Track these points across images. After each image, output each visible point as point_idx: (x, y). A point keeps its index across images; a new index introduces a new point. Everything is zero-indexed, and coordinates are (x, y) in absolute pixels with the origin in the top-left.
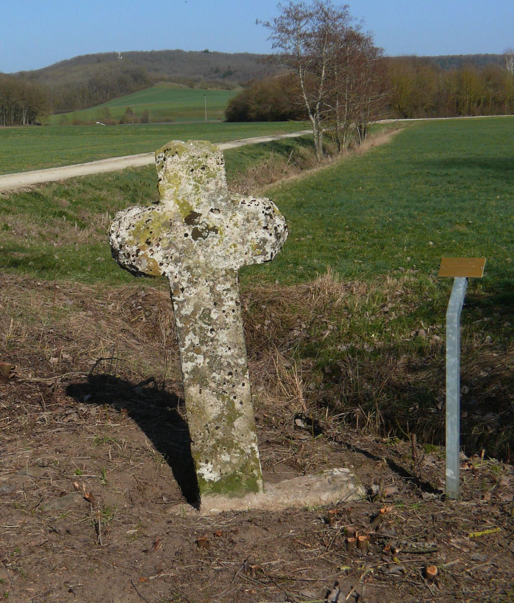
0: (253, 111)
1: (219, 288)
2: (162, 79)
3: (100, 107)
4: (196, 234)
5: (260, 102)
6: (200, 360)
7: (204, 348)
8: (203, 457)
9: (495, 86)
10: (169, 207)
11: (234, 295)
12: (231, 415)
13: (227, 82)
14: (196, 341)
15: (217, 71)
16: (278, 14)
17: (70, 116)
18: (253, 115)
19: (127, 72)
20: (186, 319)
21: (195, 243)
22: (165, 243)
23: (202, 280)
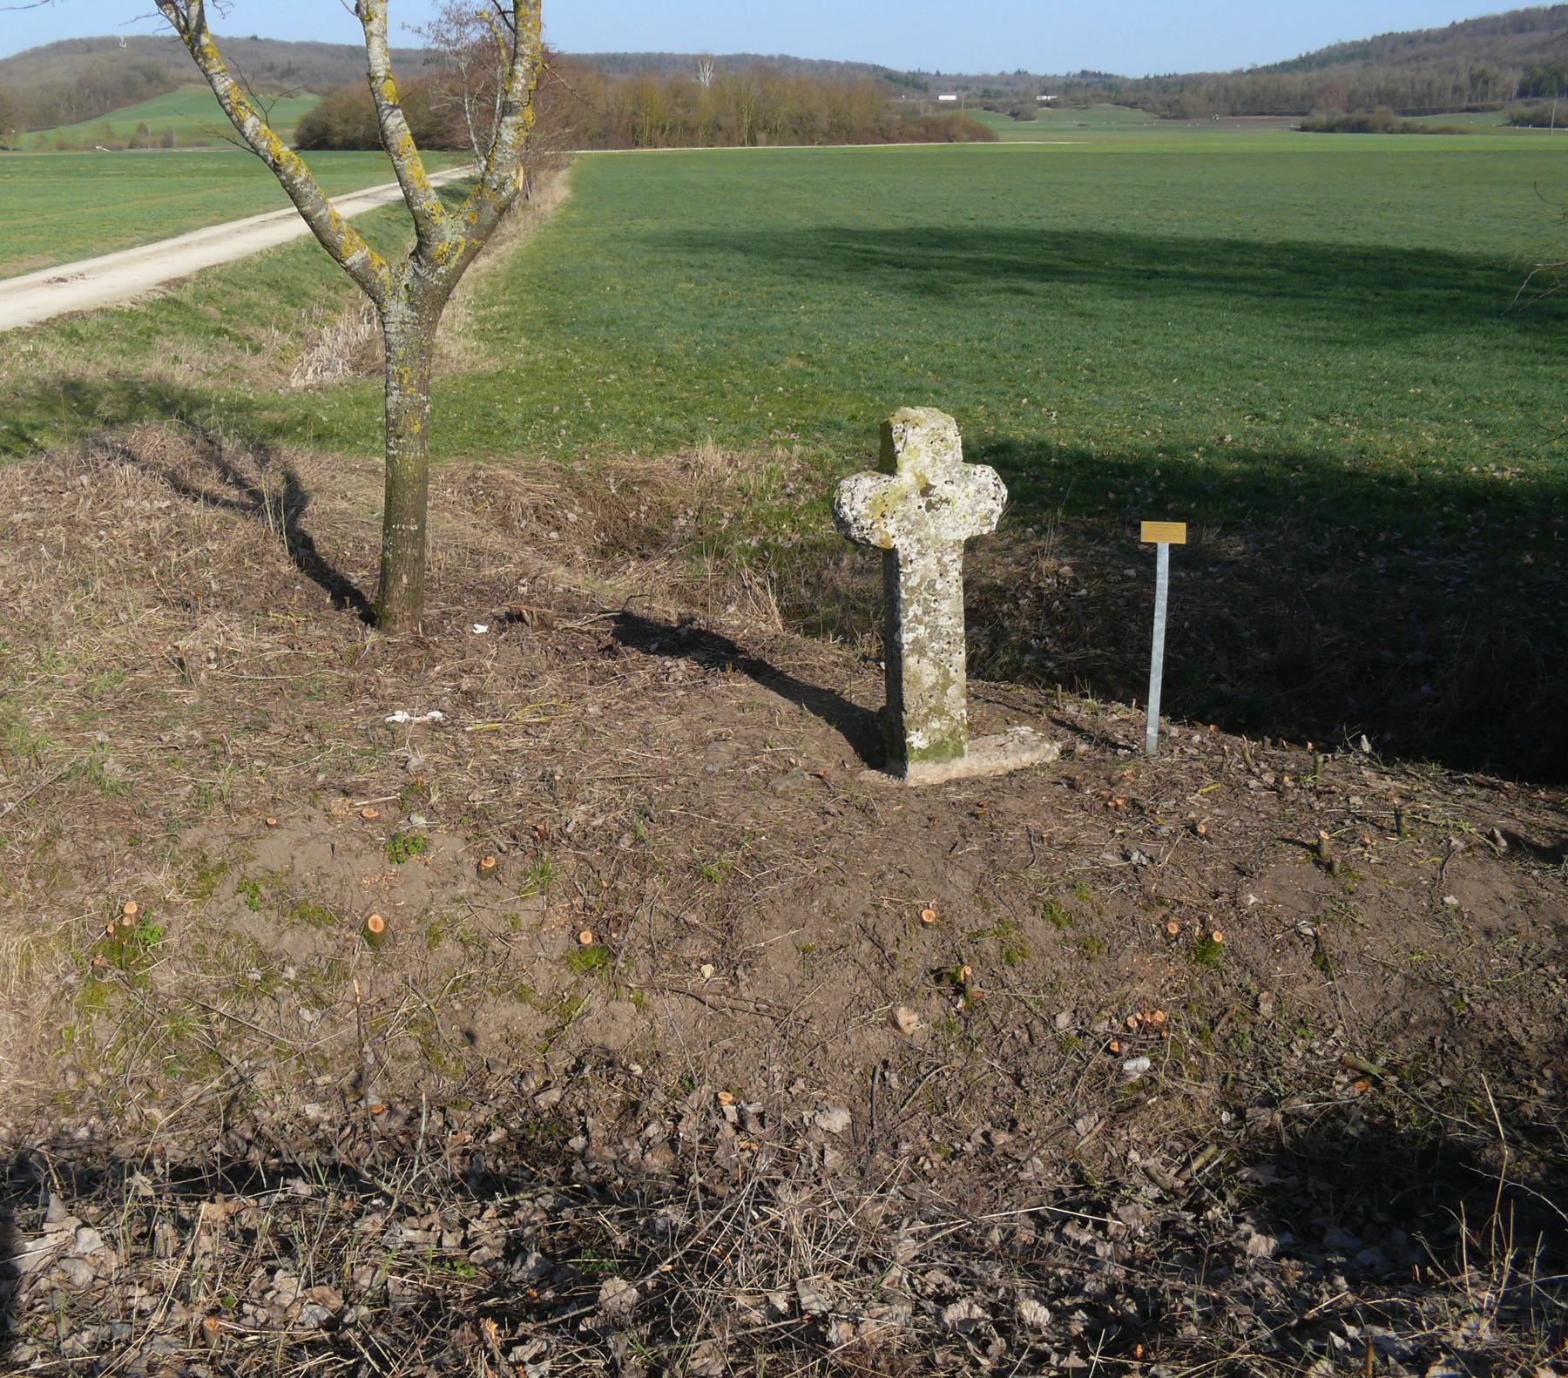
0: (336, 134)
1: (946, 559)
2: (189, 80)
3: (96, 123)
4: (930, 506)
5: (346, 121)
6: (921, 630)
7: (926, 619)
8: (914, 726)
9: (685, 105)
10: (906, 478)
11: (959, 565)
12: (946, 682)
13: (287, 85)
14: (919, 613)
15: (271, 68)
16: (435, 15)
17: (51, 134)
18: (337, 140)
19: (134, 68)
20: (912, 590)
21: (928, 515)
22: (899, 515)
23: (931, 552)
